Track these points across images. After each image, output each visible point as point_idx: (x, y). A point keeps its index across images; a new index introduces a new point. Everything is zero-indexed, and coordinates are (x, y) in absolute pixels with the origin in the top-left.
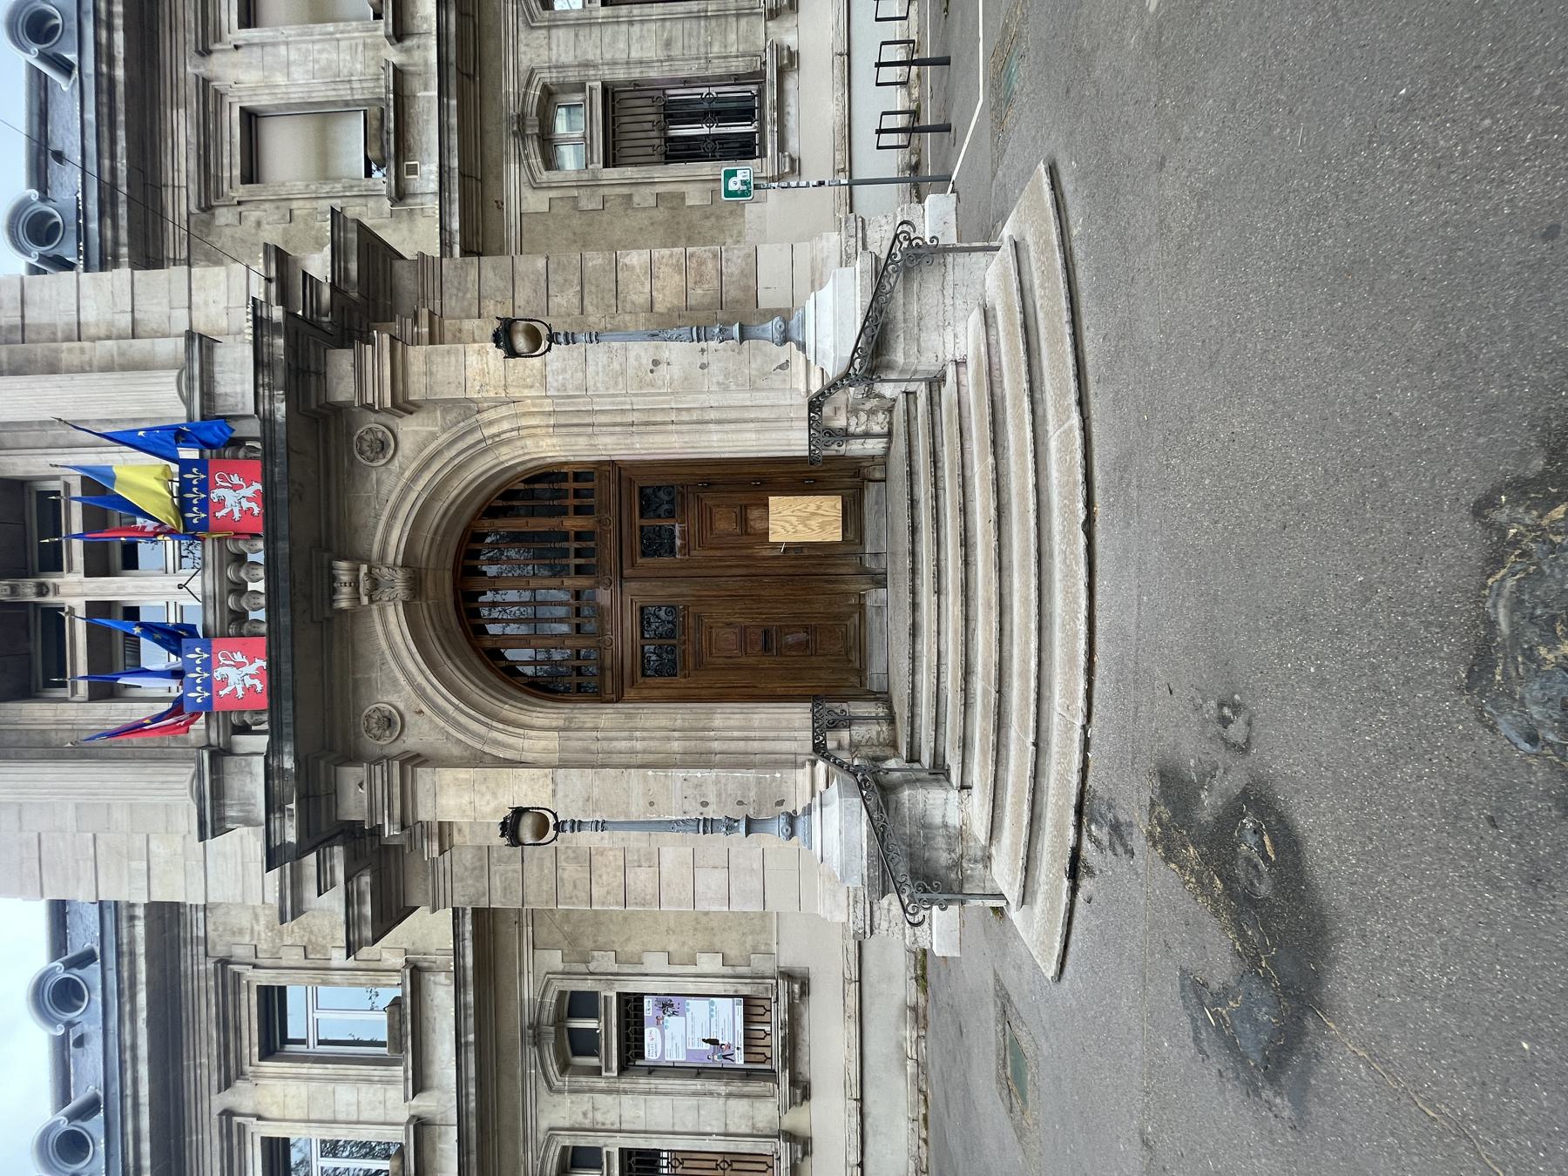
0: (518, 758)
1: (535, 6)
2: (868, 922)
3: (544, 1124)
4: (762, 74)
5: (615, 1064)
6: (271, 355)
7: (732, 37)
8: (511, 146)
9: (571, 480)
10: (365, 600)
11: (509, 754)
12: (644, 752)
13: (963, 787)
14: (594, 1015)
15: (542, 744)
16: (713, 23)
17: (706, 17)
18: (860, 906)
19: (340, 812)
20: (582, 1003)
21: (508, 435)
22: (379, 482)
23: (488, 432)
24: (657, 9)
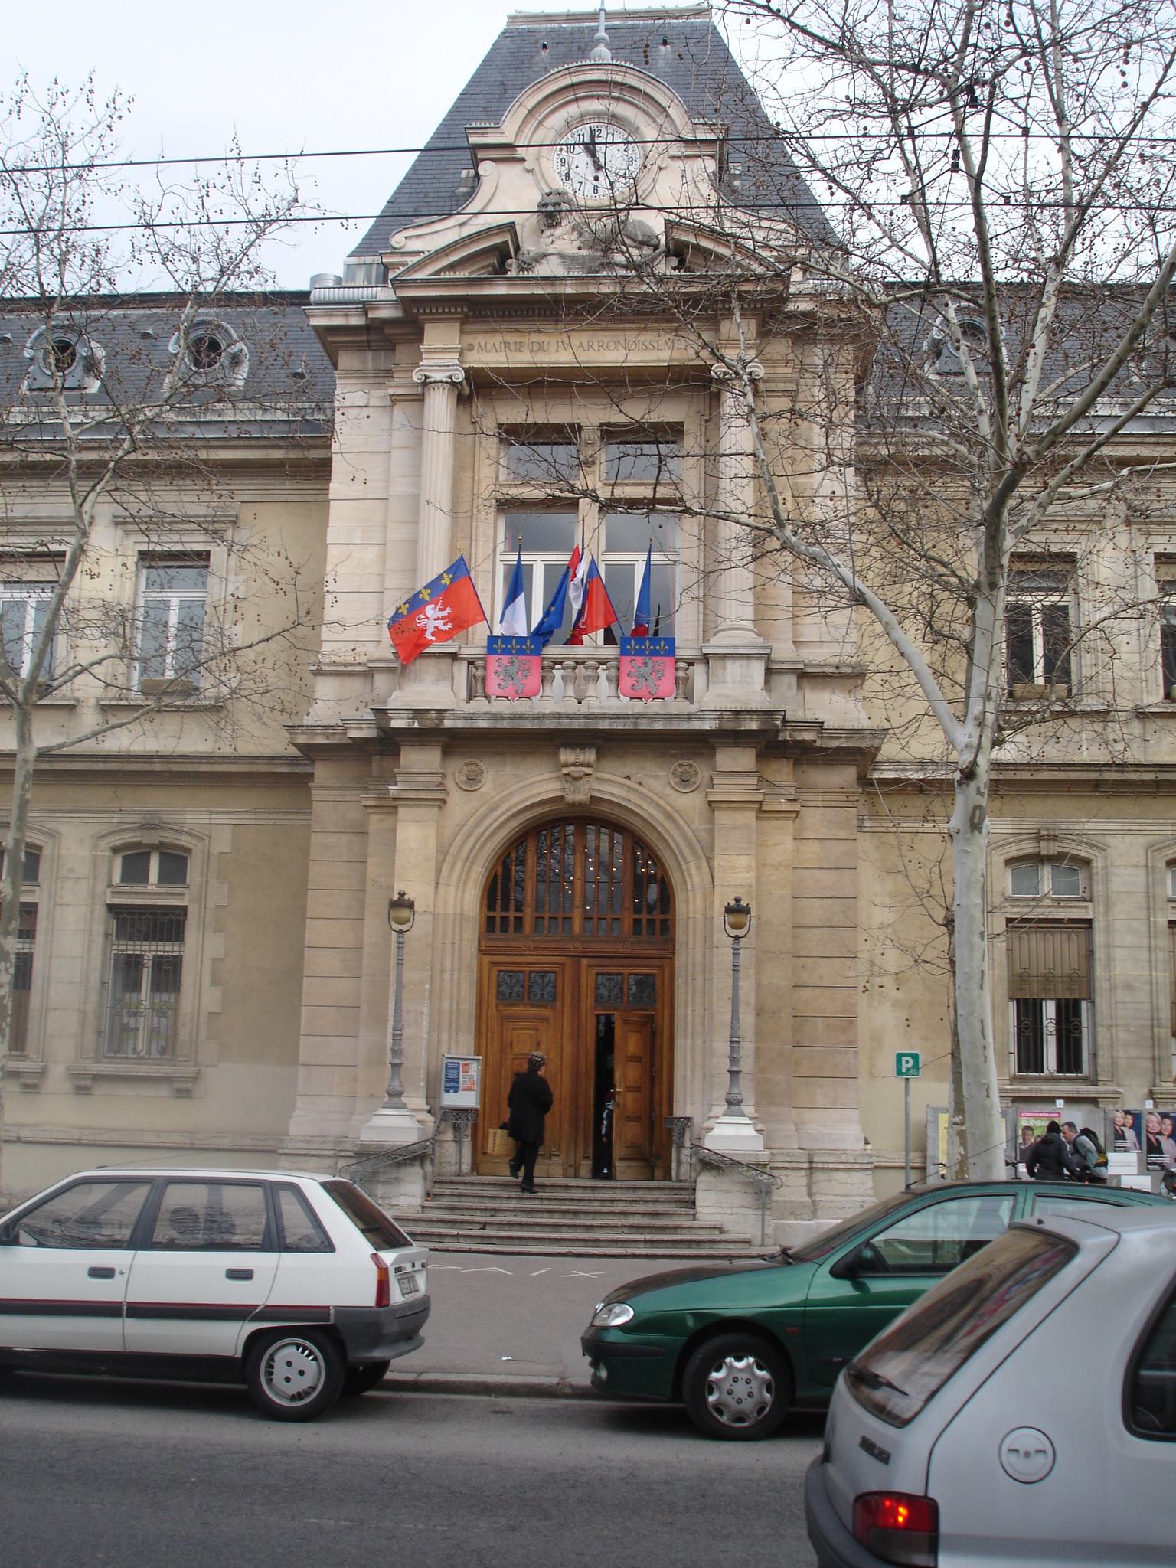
0: (441, 881)
1: (1171, 853)
2: (291, 1152)
3: (64, 829)
4: (1095, 1083)
5: (118, 901)
6: (745, 720)
7: (1133, 1052)
8: (1031, 826)
9: (662, 917)
10: (565, 771)
11: (445, 869)
12: (442, 980)
13: (423, 1207)
14: (163, 878)
15: (451, 901)
16: (1148, 1033)
17: (1152, 1027)
18: (305, 1146)
19: (407, 748)
20: (175, 864)
21: (689, 882)
22: (656, 777)
23: (692, 865)
24: (1163, 976)
